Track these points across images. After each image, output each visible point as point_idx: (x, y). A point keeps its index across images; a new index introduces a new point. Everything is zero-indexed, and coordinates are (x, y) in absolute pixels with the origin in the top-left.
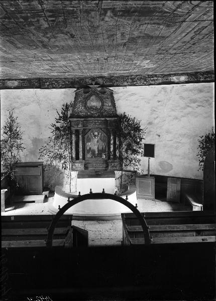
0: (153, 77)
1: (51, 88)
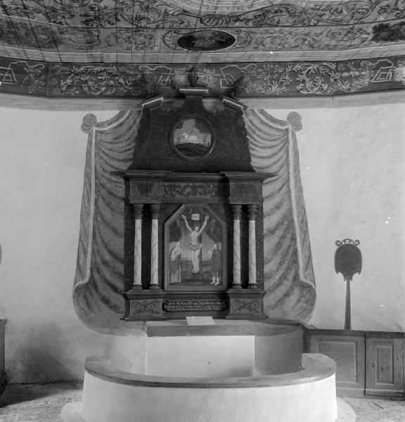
0: (348, 70)
1: (76, 97)
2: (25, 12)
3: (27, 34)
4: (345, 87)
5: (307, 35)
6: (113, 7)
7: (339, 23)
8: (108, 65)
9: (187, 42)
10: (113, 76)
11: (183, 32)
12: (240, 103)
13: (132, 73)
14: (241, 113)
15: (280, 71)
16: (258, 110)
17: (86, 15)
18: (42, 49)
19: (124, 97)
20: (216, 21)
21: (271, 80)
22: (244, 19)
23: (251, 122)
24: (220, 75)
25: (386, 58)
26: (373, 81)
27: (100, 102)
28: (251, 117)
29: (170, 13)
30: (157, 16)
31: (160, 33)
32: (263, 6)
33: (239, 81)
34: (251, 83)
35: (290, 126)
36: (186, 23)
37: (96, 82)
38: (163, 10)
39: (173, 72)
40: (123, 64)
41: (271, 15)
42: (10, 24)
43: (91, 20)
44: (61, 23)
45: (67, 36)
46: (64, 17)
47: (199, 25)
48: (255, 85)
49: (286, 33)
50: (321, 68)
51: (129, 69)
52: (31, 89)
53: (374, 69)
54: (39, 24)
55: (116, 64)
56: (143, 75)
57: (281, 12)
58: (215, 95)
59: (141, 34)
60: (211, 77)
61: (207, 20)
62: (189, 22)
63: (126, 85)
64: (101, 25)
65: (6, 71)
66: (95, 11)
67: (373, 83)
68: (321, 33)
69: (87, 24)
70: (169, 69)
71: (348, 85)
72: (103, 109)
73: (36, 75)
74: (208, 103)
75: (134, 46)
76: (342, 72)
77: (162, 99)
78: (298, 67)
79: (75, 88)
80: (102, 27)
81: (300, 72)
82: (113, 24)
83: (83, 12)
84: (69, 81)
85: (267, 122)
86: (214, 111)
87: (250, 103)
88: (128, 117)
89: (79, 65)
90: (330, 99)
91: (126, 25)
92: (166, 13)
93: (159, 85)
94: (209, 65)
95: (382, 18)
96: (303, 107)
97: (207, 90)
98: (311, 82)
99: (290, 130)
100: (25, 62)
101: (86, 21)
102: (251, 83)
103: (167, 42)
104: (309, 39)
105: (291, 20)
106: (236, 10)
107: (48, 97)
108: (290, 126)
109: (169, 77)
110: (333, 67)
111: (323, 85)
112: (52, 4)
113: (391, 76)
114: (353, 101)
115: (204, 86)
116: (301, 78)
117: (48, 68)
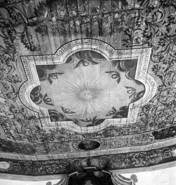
0: (152, 154)
1: (44, 175)
2: (20, 139)
3: (23, 148)
4: (153, 162)
5: (127, 139)
6: (51, 133)
7: (136, 132)
8: (55, 160)
9: (82, 146)
10: (58, 165)
11: (79, 142)
12: (109, 172)
13: (65, 163)
14: (110, 176)
15: (124, 157)
16: (118, 175)
17: (42, 138)
18: (30, 155)
19: (63, 173)
20: (89, 136)
21: (121, 161)
22: (100, 134)
23: (115, 180)
24: (100, 161)
25: (166, 147)
26: (164, 158)
27: (53, 176)
28: (115, 178)
29: (71, 134)
30: (67, 136)
31: (70, 143)
32: (104, 128)
33: (108, 163)
34: (113, 163)
35: (132, 181)
36: (78, 138)
37: (51, 168)
38: (68, 133)
39: (81, 161)
40: (61, 160)
41: (109, 132)
42: (16, 144)
43: (44, 140)
44: (34, 142)
45: (37, 148)
46: (34, 140)
47: (84, 138)
48: (115, 164)
49: (118, 139)
50: (141, 154)
51: (64, 161)
52: (27, 172)
53: (163, 153)
54: (26, 143)
55: (59, 160)
56: (70, 163)
57: (112, 130)
58: (99, 169)
59: (64, 144)
60: (96, 162)
61: (86, 136)
62: (79, 138)
63: (63, 168)
64: (48, 141)
65: (17, 165)
66: (45, 136)
67: (164, 159)
68: (133, 138)
69: (43, 142)
70: (79, 160)
71: (154, 160)
72: (54, 179)
73: (29, 167)
74: (97, 173)
75: (63, 150)
76: (150, 155)
77: (77, 172)
78: (131, 155)
79: (43, 171)
80: (49, 143)
81: (132, 157)
82: (52, 141)
83: (40, 137)
84: (41, 168)
85: (122, 179)
86: (99, 176)
87: (114, 172)
88: (64, 182)
89: (45, 161)
90: (148, 167)
91: (57, 141)
92: (70, 134)
93: (76, 167)
94: (94, 157)
95: (153, 129)
96: (137, 172)
97: (95, 167)
98: (138, 161)
99: (132, 182)
100: (24, 161)
101: (43, 140)
102: (113, 163)
103: (75, 147)
104: (129, 141)
105: (118, 133)
106: (95, 131)
107: (33, 176)
108: (132, 181)
109: (79, 163)
110: (146, 153)
111: (143, 162)
112: (29, 134)
113: (171, 155)
114: (158, 167)
115: (94, 166)
116: (133, 159)
117: (33, 163)
